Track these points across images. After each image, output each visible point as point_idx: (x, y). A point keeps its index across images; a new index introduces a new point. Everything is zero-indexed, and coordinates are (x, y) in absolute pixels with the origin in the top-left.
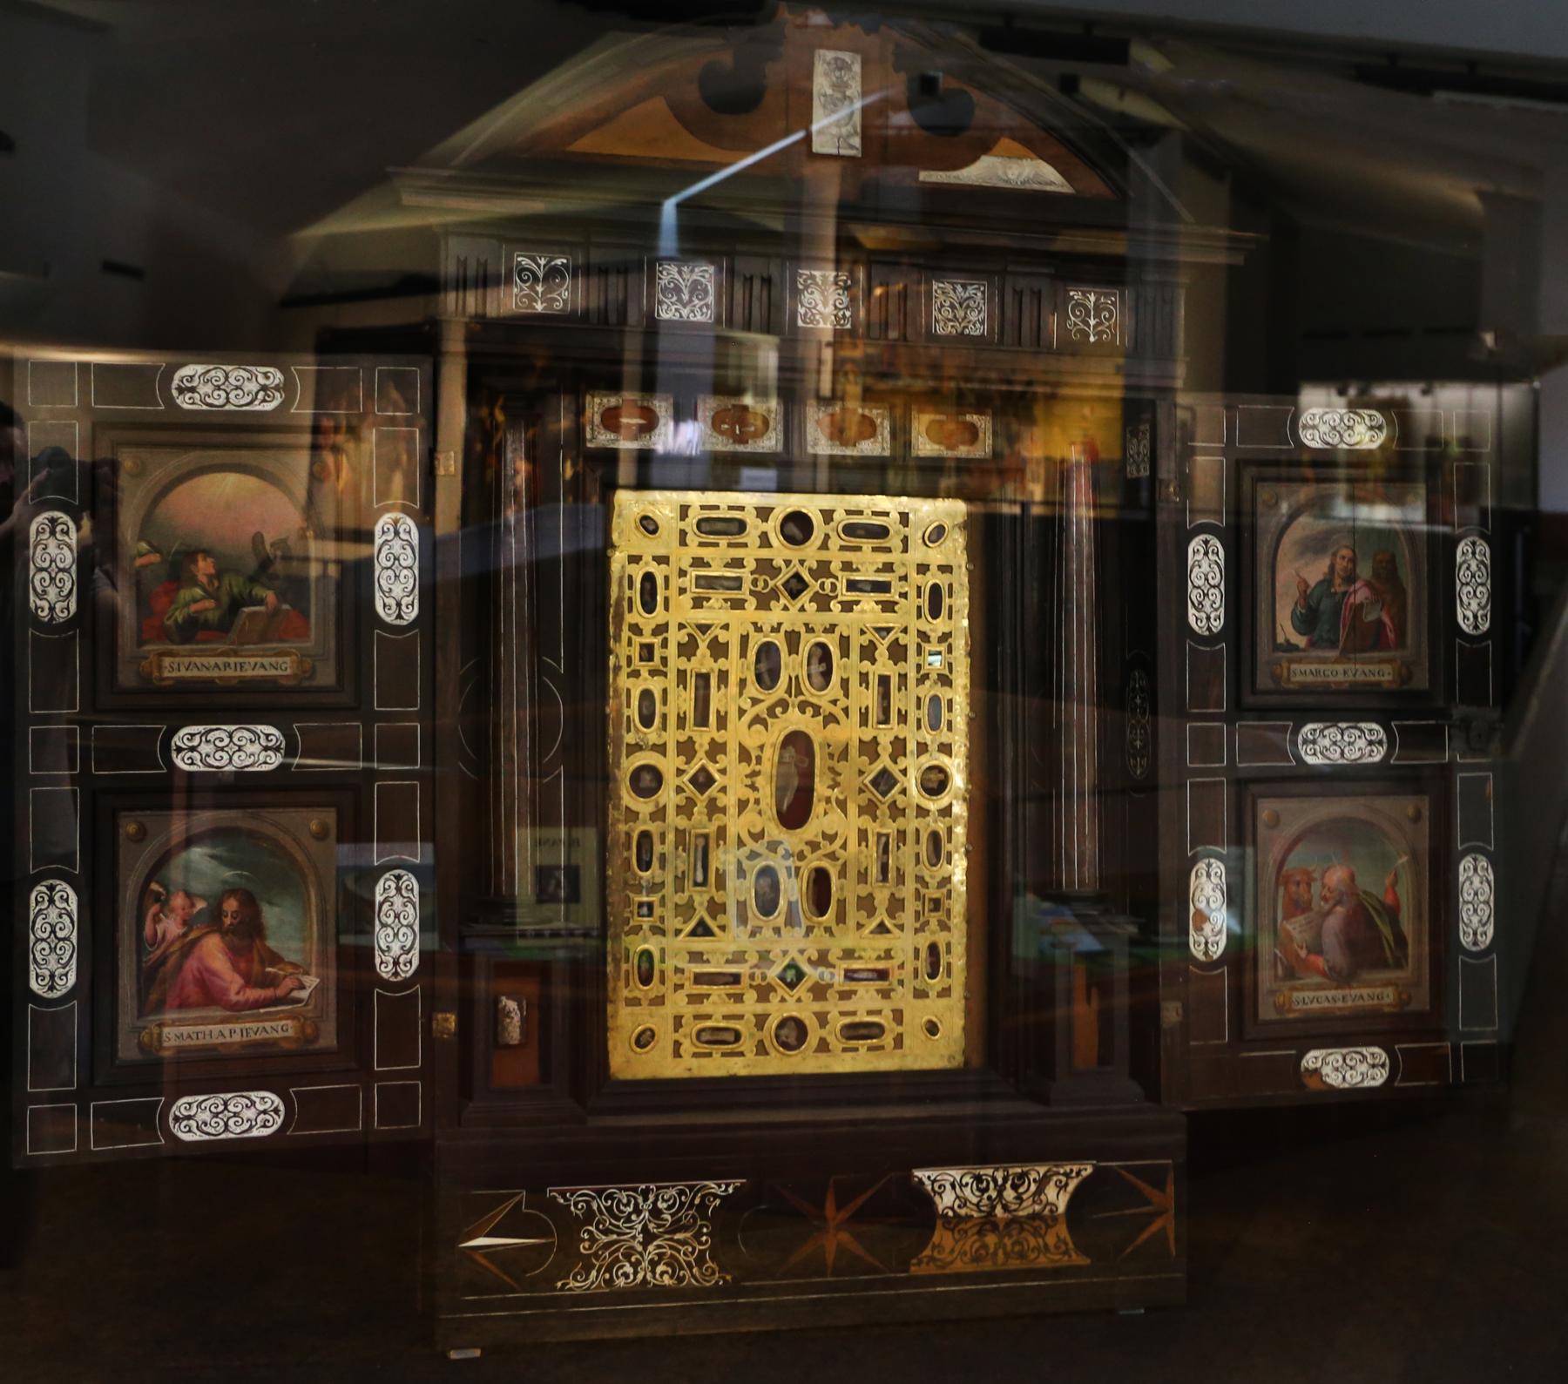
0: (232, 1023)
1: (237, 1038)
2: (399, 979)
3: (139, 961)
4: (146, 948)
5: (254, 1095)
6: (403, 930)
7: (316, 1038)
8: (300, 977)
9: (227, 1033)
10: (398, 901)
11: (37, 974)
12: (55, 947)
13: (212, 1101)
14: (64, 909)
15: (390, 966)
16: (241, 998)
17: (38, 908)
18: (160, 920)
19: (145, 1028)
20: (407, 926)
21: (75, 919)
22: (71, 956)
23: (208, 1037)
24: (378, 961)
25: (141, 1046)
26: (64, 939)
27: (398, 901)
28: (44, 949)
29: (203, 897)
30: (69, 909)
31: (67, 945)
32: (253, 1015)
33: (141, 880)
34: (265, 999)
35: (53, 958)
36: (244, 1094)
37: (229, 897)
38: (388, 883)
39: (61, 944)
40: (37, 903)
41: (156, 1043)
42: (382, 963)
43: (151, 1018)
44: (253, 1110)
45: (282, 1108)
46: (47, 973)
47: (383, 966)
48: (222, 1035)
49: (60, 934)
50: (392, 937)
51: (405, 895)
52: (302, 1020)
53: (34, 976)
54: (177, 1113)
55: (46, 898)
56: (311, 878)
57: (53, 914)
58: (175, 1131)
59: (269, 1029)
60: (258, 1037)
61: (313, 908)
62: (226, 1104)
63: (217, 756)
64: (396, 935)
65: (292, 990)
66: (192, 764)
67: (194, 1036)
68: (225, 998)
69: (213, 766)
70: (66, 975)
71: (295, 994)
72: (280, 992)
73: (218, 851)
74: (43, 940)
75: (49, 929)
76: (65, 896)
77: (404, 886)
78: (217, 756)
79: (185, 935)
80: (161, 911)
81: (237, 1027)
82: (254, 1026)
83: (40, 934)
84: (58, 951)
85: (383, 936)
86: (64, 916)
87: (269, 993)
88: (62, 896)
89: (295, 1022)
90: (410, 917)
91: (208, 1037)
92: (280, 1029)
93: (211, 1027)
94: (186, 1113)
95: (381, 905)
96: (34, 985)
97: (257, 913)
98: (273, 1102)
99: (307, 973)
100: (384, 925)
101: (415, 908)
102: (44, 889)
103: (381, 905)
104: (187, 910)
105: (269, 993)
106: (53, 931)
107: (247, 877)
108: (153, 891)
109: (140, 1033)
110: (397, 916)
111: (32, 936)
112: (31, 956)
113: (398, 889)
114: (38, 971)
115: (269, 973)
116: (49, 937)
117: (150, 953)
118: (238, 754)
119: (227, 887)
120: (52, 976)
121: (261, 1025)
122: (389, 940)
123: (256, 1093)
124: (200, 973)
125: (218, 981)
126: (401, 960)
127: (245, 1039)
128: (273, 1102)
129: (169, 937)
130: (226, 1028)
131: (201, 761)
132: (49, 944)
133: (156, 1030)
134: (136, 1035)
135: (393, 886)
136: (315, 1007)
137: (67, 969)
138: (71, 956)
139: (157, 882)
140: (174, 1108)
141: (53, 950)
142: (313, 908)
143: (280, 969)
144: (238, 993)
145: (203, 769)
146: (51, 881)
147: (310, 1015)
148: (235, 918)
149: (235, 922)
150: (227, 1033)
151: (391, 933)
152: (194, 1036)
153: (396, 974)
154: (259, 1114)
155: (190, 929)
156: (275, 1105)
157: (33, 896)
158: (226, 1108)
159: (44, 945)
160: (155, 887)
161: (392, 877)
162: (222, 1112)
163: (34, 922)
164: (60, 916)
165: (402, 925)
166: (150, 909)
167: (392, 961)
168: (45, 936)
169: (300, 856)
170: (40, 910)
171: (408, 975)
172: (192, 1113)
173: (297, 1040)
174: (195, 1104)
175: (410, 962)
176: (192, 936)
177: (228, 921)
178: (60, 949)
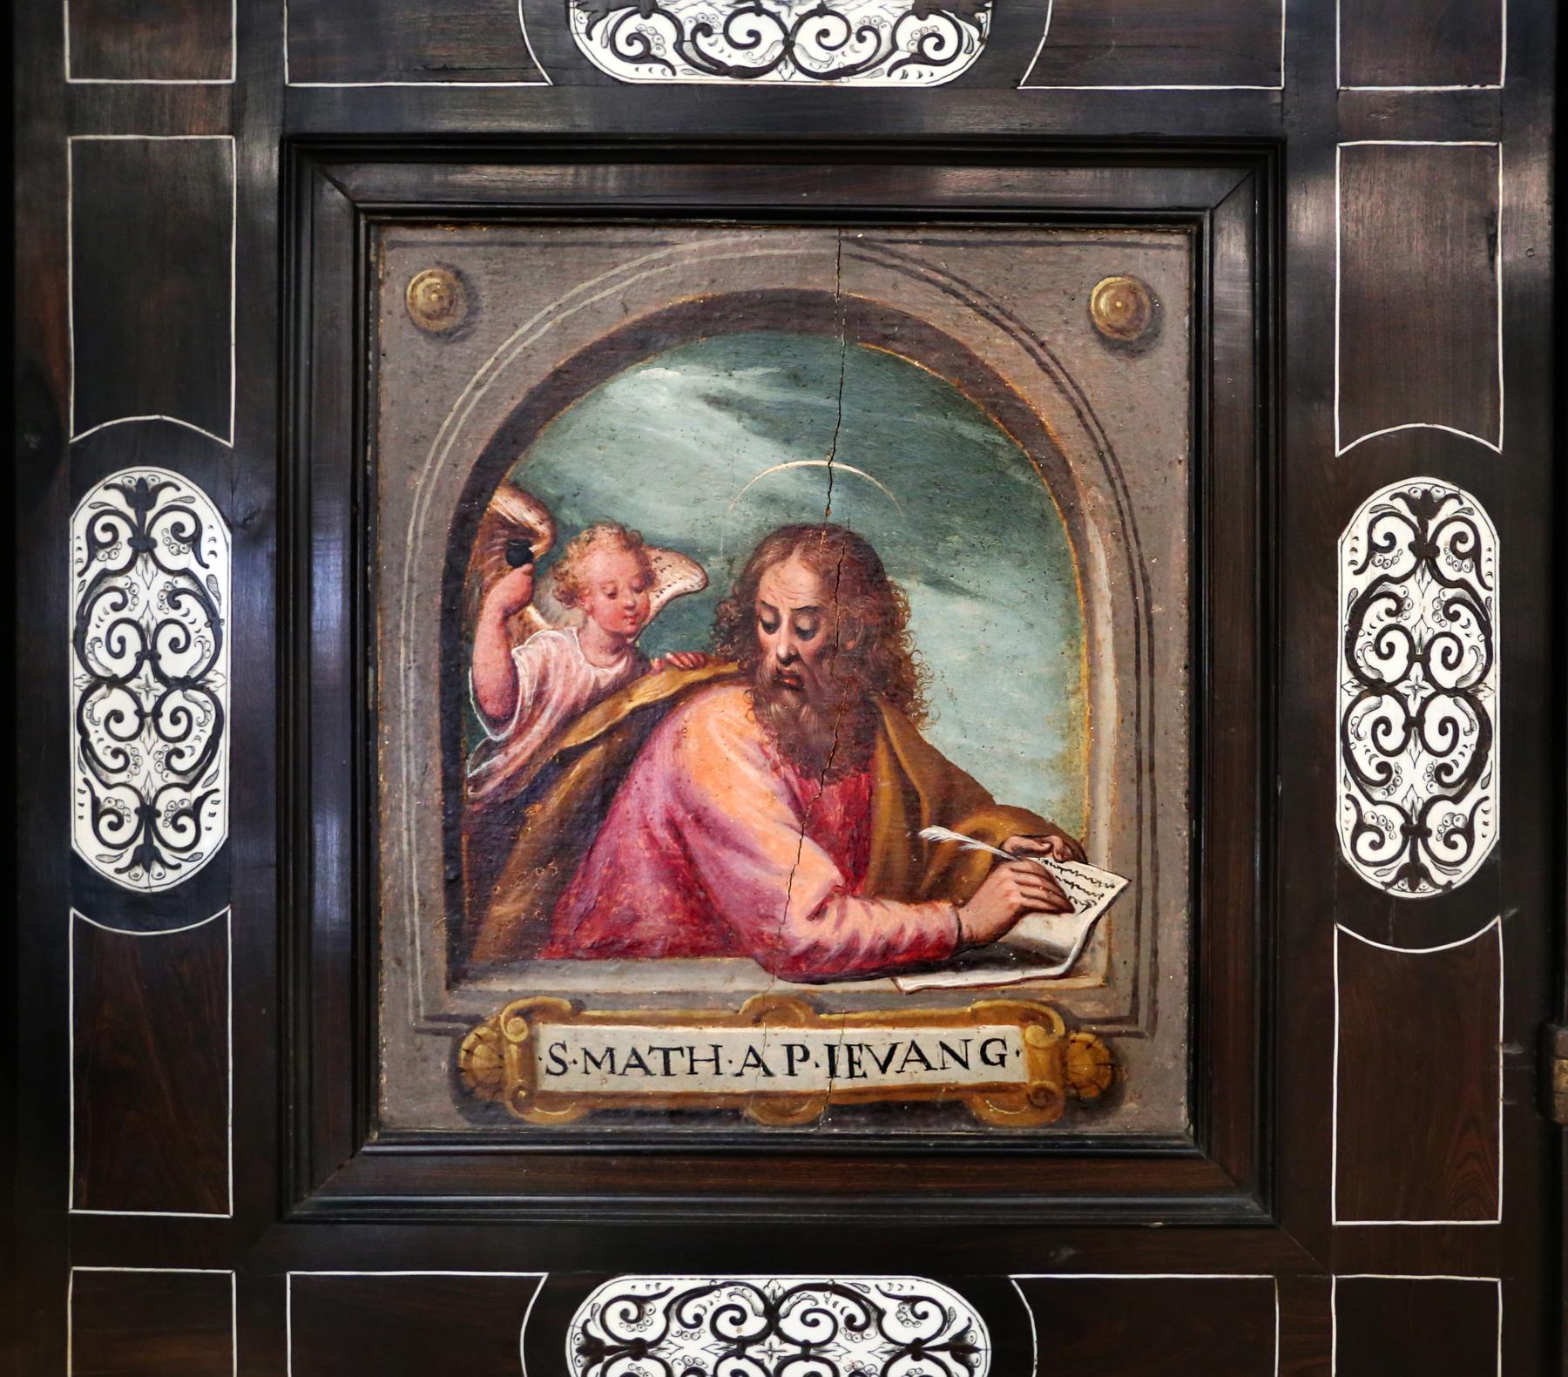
0: (795, 1023)
1: (812, 1078)
2: (1425, 891)
3: (452, 783)
4: (478, 733)
5: (875, 1286)
6: (1441, 707)
7: (1109, 1097)
8: (1051, 865)
9: (775, 1058)
10: (1423, 597)
11: (95, 802)
12: (157, 713)
13: (721, 1298)
14: (185, 572)
15: (1393, 845)
16: (828, 932)
17: (96, 567)
18: (528, 629)
19: (475, 1021)
20: (1453, 692)
21: (224, 612)
22: (212, 745)
23: (704, 1068)
24: (1345, 819)
25: (462, 1085)
26: (185, 683)
27: (1423, 597)
28: (117, 716)
29: (690, 553)
30: (202, 574)
31: (197, 704)
32: (869, 999)
33: (462, 477)
34: (920, 939)
35: (148, 749)
36: (842, 1280)
37: (784, 556)
38: (1388, 525)
39: (176, 699)
40: (94, 546)
41: (514, 1078)
42: (1360, 827)
43: (499, 986)
44: (873, 1339)
45: (980, 1338)
46: (132, 802)
47: (1366, 838)
48: (759, 1062)
49: (174, 665)
50: (1397, 736)
51: (1450, 574)
52: (1059, 1028)
53: (87, 811)
54: (595, 1331)
55: (125, 532)
56: (1094, 497)
57: (148, 588)
58: (1381, 497)
59: (933, 1054)
60: (891, 1079)
61: (1104, 612)
62: (772, 1312)
63: (739, 31)
64: (1414, 725)
65: (1024, 912)
66: (646, 57)
67: (655, 1062)
68: (768, 929)
69: (719, 68)
70: (194, 812)
71: (1033, 929)
72: (979, 916)
73: (749, 382)
74: (115, 682)
75: (134, 644)
76: (190, 529)
77: (1443, 540)
78: (739, 31)
79: (621, 687)
80: (530, 597)
81: (815, 1038)
82: (878, 1037)
83: (103, 661)
84: (165, 722)
85: (1365, 728)
86: (187, 601)
87: (934, 919)
88: (178, 528)
89: (1033, 1031)
90: (1469, 660)
91: (704, 1068)
92: (974, 1051)
93: (715, 1033)
94: (627, 1333)
95: (1360, 607)
96: (84, 842)
97: (891, 620)
98: (947, 1318)
99: (1079, 853)
100: (1467, 694)
101: (1485, 627)
102: (117, 500)
103: (1360, 607)
104: (627, 598)
105: (934, 919)
106: (149, 654)
107: (852, 482)
108: (503, 523)
109: (458, 1038)
110: (1419, 655)
111: (76, 670)
112: (75, 739)
113: (1425, 551)
114: (101, 792)
115: (936, 844)
116: (134, 674)
117: (490, 749)
118: (815, 24)
119: (776, 518)
120: (147, 813)
121: (904, 1035)
122: (1390, 743)
123: (884, 1282)
124: (673, 825)
125: (741, 867)
126: (1434, 820)
127: (842, 1083)
128: (947, 1318)
129: (560, 694)
130: (773, 1039)
131: (678, 46)
132: (135, 697)
133: (514, 1031)
134: (446, 1043)
135: (1405, 536)
136: (1109, 979)
137: (198, 791)
138: (212, 746)
139: (518, 489)
140: (583, 1313)
141: (149, 718)
142: (1104, 612)
143: (977, 835)
144: (818, 913)
145: (686, 76)
146: (137, 473)
147: (1089, 1009)
148: (803, 634)
149: (806, 647)
150: (775, 1058)
151: (1397, 718)
152: (655, 1062)
153: (1414, 873)
154: (896, 1357)
155: (640, 667)
156: (956, 1327)
157: (79, 524)
158: (773, 1327)
159: (118, 700)
160: (507, 504)
161: (1400, 505)
162: (759, 1338)
163: (84, 619)
164: (173, 598)
165: (1440, 690)
166: (485, 591)
167: (1399, 820)
168: (122, 667)
169: (1052, 411)
170: (105, 574)
171: (1461, 877)
172: (650, 1335)
173: (1038, 1098)
174: (661, 1304)
175: (1468, 832)
176: (649, 691)
177: (778, 644)
178: (175, 720)
